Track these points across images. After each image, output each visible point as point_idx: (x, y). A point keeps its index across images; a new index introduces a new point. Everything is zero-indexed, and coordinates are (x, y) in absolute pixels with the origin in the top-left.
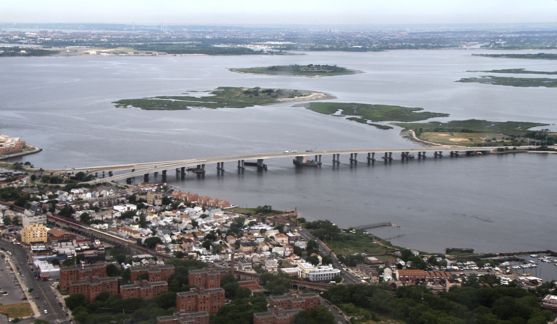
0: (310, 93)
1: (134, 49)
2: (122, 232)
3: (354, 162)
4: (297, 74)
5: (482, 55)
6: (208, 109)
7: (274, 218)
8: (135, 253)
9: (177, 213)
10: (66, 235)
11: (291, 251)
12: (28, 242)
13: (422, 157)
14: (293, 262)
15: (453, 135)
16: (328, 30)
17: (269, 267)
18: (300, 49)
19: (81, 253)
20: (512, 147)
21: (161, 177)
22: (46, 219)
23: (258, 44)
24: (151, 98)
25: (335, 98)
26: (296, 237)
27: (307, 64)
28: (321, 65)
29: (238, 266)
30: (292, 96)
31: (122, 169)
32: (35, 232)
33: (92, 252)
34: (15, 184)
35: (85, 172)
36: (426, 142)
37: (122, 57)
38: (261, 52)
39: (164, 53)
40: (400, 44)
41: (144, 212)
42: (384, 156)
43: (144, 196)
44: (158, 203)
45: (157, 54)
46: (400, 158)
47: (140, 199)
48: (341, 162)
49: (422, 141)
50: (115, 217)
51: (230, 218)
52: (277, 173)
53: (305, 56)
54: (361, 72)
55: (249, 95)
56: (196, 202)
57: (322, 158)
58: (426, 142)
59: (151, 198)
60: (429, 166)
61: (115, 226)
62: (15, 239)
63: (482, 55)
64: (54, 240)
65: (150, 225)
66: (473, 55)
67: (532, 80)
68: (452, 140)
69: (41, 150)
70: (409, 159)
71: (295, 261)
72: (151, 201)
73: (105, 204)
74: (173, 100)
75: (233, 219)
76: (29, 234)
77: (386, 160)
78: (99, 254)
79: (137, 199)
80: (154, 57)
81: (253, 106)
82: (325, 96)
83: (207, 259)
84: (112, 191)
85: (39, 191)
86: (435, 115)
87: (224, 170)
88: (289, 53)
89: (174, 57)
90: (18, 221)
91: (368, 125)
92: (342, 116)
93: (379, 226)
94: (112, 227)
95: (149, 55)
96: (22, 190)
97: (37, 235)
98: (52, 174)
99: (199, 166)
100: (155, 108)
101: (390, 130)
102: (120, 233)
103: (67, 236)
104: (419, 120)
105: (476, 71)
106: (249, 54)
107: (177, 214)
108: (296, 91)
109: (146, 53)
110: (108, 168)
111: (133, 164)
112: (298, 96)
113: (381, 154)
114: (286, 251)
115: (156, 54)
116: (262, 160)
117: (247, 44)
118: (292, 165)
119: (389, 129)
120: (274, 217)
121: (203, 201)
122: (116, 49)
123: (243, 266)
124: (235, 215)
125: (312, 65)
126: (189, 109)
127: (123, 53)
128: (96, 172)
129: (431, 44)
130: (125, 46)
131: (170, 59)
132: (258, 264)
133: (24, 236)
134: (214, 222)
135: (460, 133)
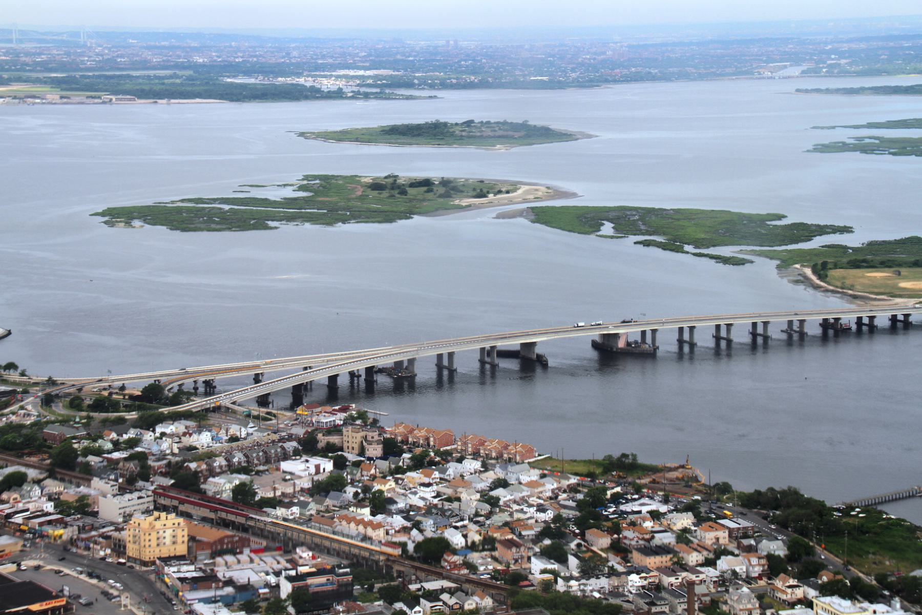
0: (513, 187)
1: (52, 87)
2: (341, 525)
3: (723, 344)
4: (454, 143)
5: (818, 91)
6: (317, 227)
7: (650, 482)
8: (414, 577)
9: (433, 476)
10: (228, 537)
11: (763, 565)
12: (147, 556)
13: (865, 328)
14: (784, 592)
15: (899, 273)
16: (452, 42)
17: (741, 607)
18: (419, 85)
19: (301, 583)
21: (326, 390)
22: (151, 499)
23: (325, 76)
24: (173, 202)
25: (574, 195)
26: (744, 528)
27: (461, 118)
28: (492, 121)
29: (667, 607)
30: (482, 195)
31: (235, 375)
32: (161, 532)
33: (322, 580)
34: (11, 415)
35: (163, 380)
36: (850, 292)
37: (36, 106)
38: (338, 95)
39: (128, 97)
40: (625, 71)
41: (356, 475)
42: (785, 327)
43: (335, 437)
44: (375, 452)
45: (114, 100)
46: (818, 331)
47: (328, 443)
48: (699, 344)
49: (840, 290)
50: (299, 489)
51: (560, 485)
52: (571, 372)
53: (437, 100)
54: (590, 136)
55: (385, 194)
56: (453, 447)
57: (658, 335)
58: (850, 292)
59: (354, 440)
60: (882, 347)
61: (313, 512)
62: (108, 551)
63: (818, 91)
64: (203, 549)
65: (393, 508)
66: (798, 90)
68: (904, 284)
69: (9, 333)
70: (840, 333)
71: (789, 591)
72: (353, 448)
73: (258, 459)
74: (226, 207)
75: (566, 487)
76: (147, 538)
77: (790, 337)
78: (340, 585)
79: (321, 445)
80: (108, 106)
81: (412, 218)
82: (550, 191)
83: (582, 587)
84: (252, 425)
85: (85, 430)
86: (822, 230)
87: (455, 370)
88: (402, 95)
89: (153, 105)
90: (88, 505)
91: (692, 256)
92: (618, 237)
93: (903, 498)
94: (308, 513)
95: (96, 101)
96: (45, 431)
97: (164, 541)
98: (80, 390)
99: (399, 364)
100: (199, 225)
101: (747, 265)
102: (338, 527)
103: (230, 539)
104: (797, 242)
105: (834, 127)
106: (306, 98)
107: (433, 479)
108: (482, 182)
109: (88, 97)
110: (204, 371)
111: (258, 362)
112: (495, 194)
113: (781, 323)
114: (750, 564)
115: (111, 100)
116: (534, 344)
117: (299, 75)
118: (593, 354)
119: (746, 265)
120: (651, 480)
121: (470, 445)
122: (10, 88)
123: (679, 606)
124: (568, 479)
125: (472, 121)
126: (276, 228)
127: (34, 97)
128: (155, 379)
129: (675, 70)
130: (25, 81)
131: (143, 107)
132: (708, 599)
133: (135, 542)
134: (529, 497)
135: (911, 269)
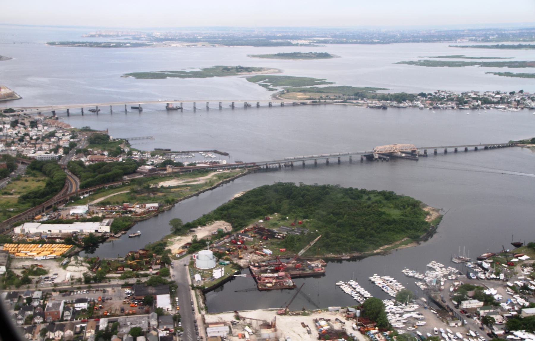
48: (197, 108)
54: (337, 57)
66: (450, 46)
67: (449, 62)
105: (161, 76)
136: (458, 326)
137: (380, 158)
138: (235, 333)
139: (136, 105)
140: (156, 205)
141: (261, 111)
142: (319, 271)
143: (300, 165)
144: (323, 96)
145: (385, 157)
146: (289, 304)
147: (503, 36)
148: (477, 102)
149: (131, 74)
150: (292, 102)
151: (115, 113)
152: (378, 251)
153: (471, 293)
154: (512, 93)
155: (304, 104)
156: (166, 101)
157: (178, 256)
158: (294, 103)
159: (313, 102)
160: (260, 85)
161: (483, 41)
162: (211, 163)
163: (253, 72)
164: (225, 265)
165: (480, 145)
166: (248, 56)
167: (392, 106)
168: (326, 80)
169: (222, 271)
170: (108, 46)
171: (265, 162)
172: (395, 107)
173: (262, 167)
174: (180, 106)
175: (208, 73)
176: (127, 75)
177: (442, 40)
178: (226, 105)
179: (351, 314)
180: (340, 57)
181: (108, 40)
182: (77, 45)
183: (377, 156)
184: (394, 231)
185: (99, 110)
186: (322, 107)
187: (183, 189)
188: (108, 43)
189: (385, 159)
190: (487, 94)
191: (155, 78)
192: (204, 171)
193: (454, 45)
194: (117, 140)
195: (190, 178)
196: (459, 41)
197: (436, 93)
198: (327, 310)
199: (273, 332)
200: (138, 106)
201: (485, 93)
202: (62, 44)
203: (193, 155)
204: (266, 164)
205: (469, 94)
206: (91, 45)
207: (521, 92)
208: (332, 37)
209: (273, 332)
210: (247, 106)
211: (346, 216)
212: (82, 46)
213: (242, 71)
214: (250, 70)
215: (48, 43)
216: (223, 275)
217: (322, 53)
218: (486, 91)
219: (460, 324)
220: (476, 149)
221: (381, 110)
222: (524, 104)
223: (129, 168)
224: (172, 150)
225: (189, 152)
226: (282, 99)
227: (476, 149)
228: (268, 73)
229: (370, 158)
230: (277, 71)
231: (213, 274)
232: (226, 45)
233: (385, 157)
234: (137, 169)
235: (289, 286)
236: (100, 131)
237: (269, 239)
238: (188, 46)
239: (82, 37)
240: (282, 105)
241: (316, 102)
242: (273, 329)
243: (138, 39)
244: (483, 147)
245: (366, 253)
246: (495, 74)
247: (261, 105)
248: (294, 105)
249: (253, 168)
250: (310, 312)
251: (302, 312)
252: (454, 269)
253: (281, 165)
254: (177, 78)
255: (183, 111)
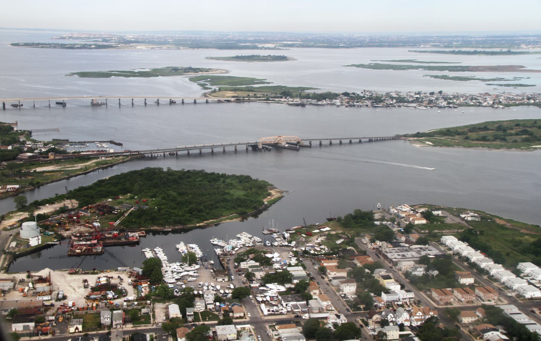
20: (248, 98)
54: (294, 59)
66: (409, 51)
67: (397, 66)
104: (249, 85)
136: (225, 281)
137: (263, 148)
138: (17, 288)
139: (60, 100)
140: (17, 186)
141: (185, 107)
142: (133, 240)
143: (197, 154)
144: (251, 94)
145: (267, 147)
146: (80, 265)
147: (466, 42)
148: (392, 101)
149: (75, 74)
150: (217, 100)
151: (37, 108)
152: (201, 224)
153: (251, 256)
154: (432, 94)
155: (228, 101)
156: (91, 97)
157: (9, 228)
158: (218, 100)
159: (237, 100)
160: (198, 84)
161: (445, 47)
162: (98, 151)
163: (200, 73)
164: (48, 235)
165: (364, 138)
166: (207, 58)
167: (311, 104)
168: (266, 80)
169: (39, 239)
170: (72, 47)
171: (150, 151)
172: (313, 104)
173: (146, 155)
174: (105, 103)
175: (155, 73)
176: (73, 74)
177: (407, 45)
178: (151, 101)
179: (134, 273)
180: (296, 60)
181: (71, 42)
182: (40, 46)
183: (260, 147)
184: (225, 208)
185: (22, 105)
186: (246, 105)
187: (56, 174)
188: (73, 44)
189: (267, 149)
190: (409, 94)
191: (99, 77)
192: (87, 158)
193: (414, 50)
194: (20, 132)
195: (69, 164)
196: (422, 46)
197: (362, 93)
198: (117, 270)
199: (47, 286)
200: (62, 102)
201: (408, 93)
202: (26, 45)
203: (88, 145)
204: (151, 153)
205: (391, 94)
206: (55, 46)
207: (440, 92)
208: (301, 41)
209: (47, 286)
210: (172, 103)
211: (190, 196)
212: (46, 47)
213: (189, 71)
214: (197, 71)
215: (12, 44)
216: (40, 243)
217: (280, 56)
218: (408, 91)
219: (226, 279)
220: (360, 142)
221: (300, 107)
222: (435, 103)
223: (9, 155)
224: (70, 141)
225: (85, 142)
226: (210, 97)
227: (360, 142)
228: (214, 74)
229: (255, 148)
230: (224, 71)
231: (29, 242)
232: (190, 48)
233: (267, 147)
234: (17, 156)
235: (97, 252)
236: (9, 124)
237: (106, 215)
238: (152, 48)
239: (52, 38)
240: (207, 102)
241: (240, 100)
242: (48, 283)
243: (107, 41)
244: (368, 140)
245: (188, 226)
246: (432, 76)
247: (185, 101)
248: (219, 102)
249: (137, 156)
250: (99, 272)
251: (92, 271)
252: (259, 239)
253: (166, 153)
254: (122, 78)
255: (108, 107)
